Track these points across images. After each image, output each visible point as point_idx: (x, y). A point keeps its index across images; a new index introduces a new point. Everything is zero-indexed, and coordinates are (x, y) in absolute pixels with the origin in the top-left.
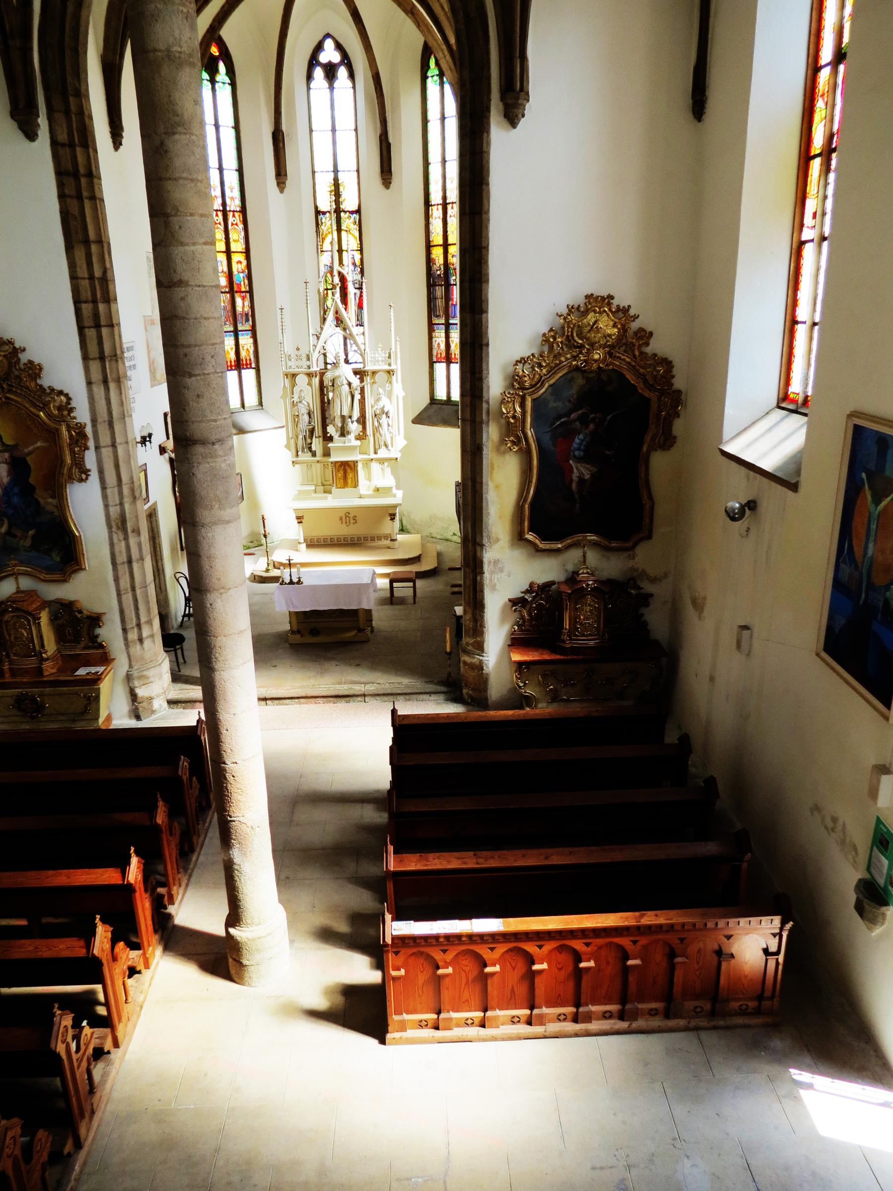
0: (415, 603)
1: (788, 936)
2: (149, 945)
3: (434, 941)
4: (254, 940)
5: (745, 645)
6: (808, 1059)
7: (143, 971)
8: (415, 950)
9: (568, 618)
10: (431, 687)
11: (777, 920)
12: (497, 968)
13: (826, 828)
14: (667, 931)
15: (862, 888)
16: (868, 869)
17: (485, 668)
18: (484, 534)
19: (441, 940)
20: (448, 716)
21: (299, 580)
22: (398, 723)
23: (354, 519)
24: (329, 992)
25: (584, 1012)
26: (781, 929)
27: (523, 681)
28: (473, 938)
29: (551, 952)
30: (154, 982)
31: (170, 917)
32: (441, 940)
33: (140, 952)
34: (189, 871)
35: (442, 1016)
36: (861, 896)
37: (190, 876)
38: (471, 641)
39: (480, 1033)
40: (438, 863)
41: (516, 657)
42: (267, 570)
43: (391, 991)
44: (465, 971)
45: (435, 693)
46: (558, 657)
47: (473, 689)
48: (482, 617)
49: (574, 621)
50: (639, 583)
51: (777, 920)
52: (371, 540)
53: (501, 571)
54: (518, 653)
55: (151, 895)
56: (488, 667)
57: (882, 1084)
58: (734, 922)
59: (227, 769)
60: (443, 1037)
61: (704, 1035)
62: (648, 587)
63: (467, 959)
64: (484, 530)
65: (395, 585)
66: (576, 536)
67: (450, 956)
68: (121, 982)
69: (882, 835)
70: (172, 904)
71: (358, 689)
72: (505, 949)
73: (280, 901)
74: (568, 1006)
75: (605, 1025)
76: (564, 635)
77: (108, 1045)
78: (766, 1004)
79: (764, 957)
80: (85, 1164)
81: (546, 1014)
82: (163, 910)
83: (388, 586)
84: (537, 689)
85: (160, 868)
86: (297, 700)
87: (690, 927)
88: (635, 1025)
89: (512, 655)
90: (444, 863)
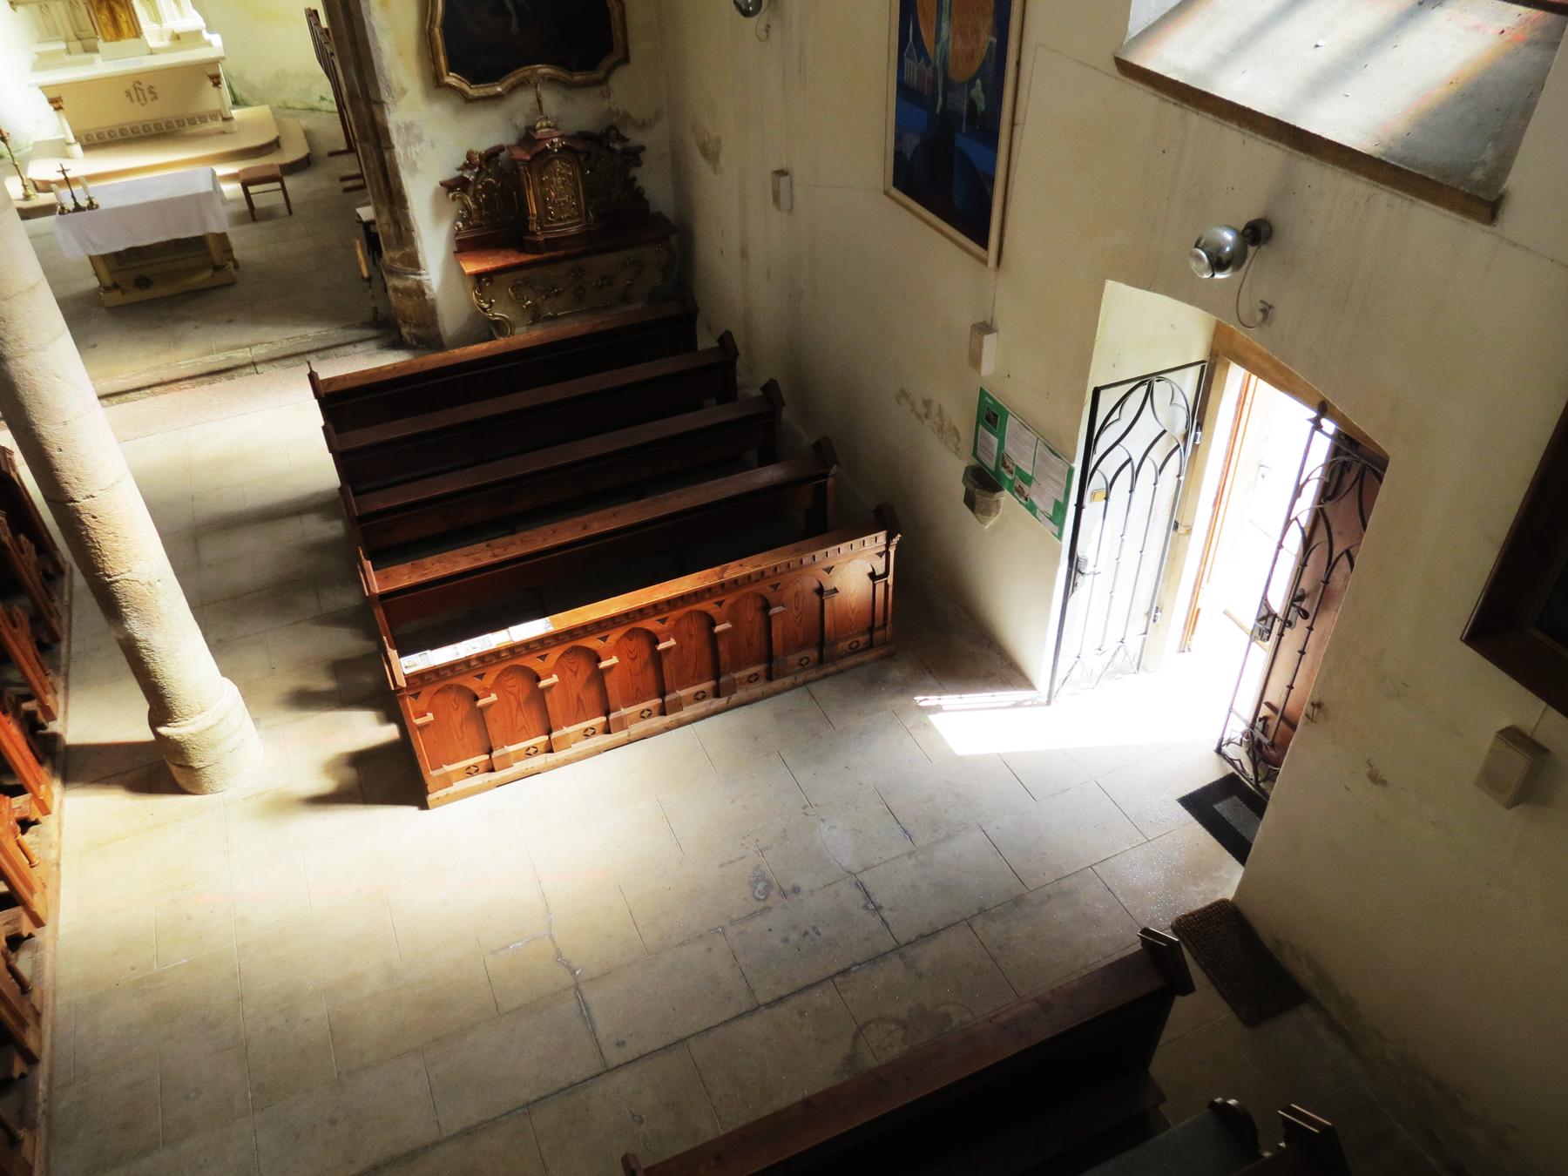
0: (290, 213)
1: (895, 552)
2: (39, 784)
3: (464, 667)
4: (201, 733)
5: (784, 199)
6: (931, 681)
7: (42, 819)
8: (440, 685)
9: (532, 198)
10: (354, 334)
11: (882, 536)
12: (555, 679)
13: (919, 416)
14: (757, 581)
15: (971, 478)
16: (975, 454)
17: (427, 291)
18: (381, 84)
19: (473, 663)
20: (395, 367)
21: (91, 203)
22: (322, 392)
23: (151, 92)
24: (331, 767)
25: (671, 701)
26: (888, 546)
27: (488, 300)
28: (514, 650)
29: (618, 641)
30: (64, 829)
31: (55, 737)
32: (473, 663)
33: (27, 796)
34: (63, 669)
35: (495, 754)
36: (972, 488)
37: (67, 675)
38: (397, 255)
39: (548, 760)
40: (440, 568)
41: (471, 267)
42: (27, 197)
43: (420, 744)
44: (513, 694)
45: (362, 341)
46: (530, 257)
47: (417, 326)
48: (406, 217)
49: (543, 202)
50: (622, 132)
51: (882, 536)
52: (201, 122)
53: (420, 139)
54: (472, 261)
55: (16, 716)
56: (430, 289)
57: (1011, 685)
58: (834, 550)
59: (80, 508)
60: (502, 777)
61: (814, 687)
62: (636, 138)
63: (512, 678)
64: (380, 78)
65: (251, 189)
66: (520, 70)
67: (489, 680)
68: (14, 845)
69: (988, 408)
70: (52, 720)
71: (241, 356)
72: (561, 652)
73: (224, 674)
74: (651, 699)
75: (700, 707)
76: (532, 224)
77: (26, 927)
78: (878, 634)
79: (871, 582)
80: (51, 1077)
81: (626, 715)
82: (40, 731)
83: (241, 193)
84: (509, 309)
85: (14, 675)
86: (148, 391)
87: (784, 569)
88: (734, 698)
89: (463, 265)
90: (448, 566)
